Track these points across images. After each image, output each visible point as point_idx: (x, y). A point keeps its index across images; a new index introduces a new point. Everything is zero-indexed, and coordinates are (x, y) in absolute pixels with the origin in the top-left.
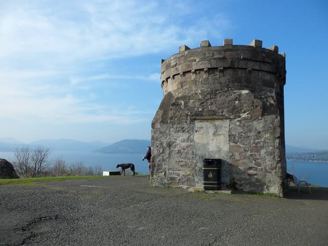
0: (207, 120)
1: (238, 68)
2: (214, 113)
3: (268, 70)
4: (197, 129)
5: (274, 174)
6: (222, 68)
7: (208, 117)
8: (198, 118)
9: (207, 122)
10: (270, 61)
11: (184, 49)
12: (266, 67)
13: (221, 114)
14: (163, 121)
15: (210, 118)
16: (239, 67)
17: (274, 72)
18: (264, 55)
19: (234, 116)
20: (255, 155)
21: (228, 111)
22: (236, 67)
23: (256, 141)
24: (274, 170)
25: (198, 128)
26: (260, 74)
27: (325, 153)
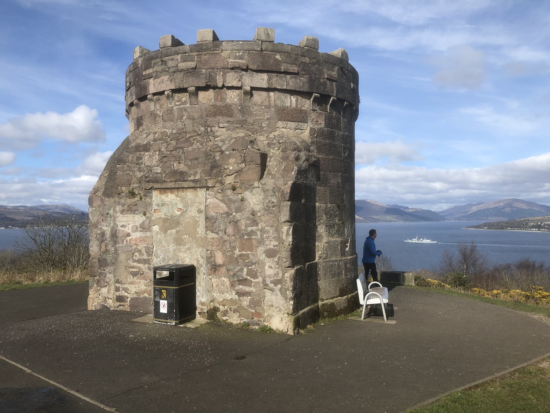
0: (171, 189)
1: (223, 86)
2: (181, 176)
3: (288, 88)
4: (156, 208)
5: (279, 294)
6: (194, 88)
7: (172, 185)
8: (156, 186)
9: (172, 193)
10: (294, 69)
11: (169, 43)
12: (290, 82)
13: (192, 178)
14: (108, 193)
15: (163, 187)
16: (227, 85)
17: (306, 89)
18: (278, 57)
19: (212, 181)
20: (247, 256)
21: (204, 172)
22: (220, 85)
23: (250, 229)
24: (279, 286)
25: (158, 205)
26: (272, 94)
27: (510, 218)
